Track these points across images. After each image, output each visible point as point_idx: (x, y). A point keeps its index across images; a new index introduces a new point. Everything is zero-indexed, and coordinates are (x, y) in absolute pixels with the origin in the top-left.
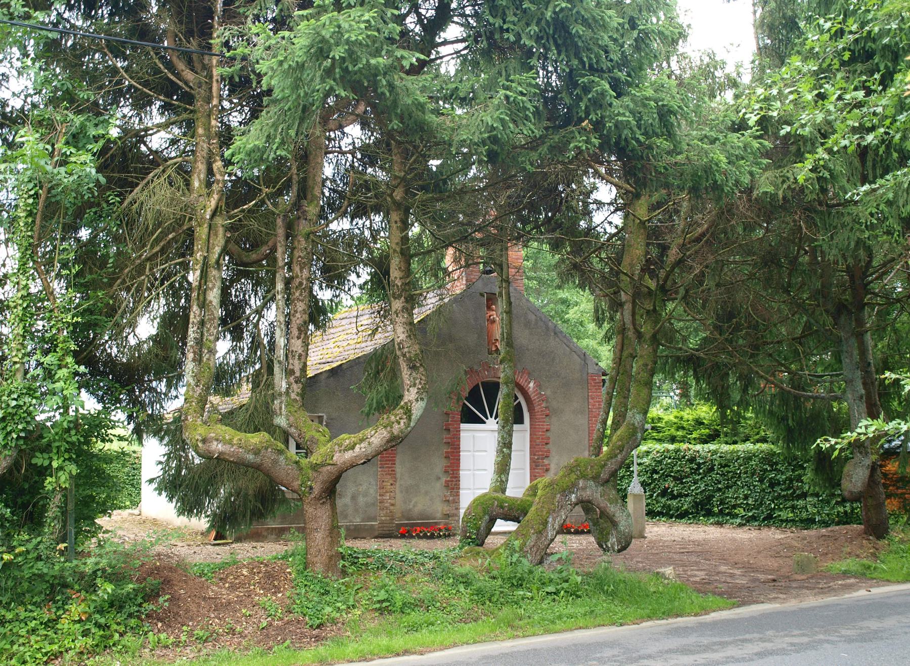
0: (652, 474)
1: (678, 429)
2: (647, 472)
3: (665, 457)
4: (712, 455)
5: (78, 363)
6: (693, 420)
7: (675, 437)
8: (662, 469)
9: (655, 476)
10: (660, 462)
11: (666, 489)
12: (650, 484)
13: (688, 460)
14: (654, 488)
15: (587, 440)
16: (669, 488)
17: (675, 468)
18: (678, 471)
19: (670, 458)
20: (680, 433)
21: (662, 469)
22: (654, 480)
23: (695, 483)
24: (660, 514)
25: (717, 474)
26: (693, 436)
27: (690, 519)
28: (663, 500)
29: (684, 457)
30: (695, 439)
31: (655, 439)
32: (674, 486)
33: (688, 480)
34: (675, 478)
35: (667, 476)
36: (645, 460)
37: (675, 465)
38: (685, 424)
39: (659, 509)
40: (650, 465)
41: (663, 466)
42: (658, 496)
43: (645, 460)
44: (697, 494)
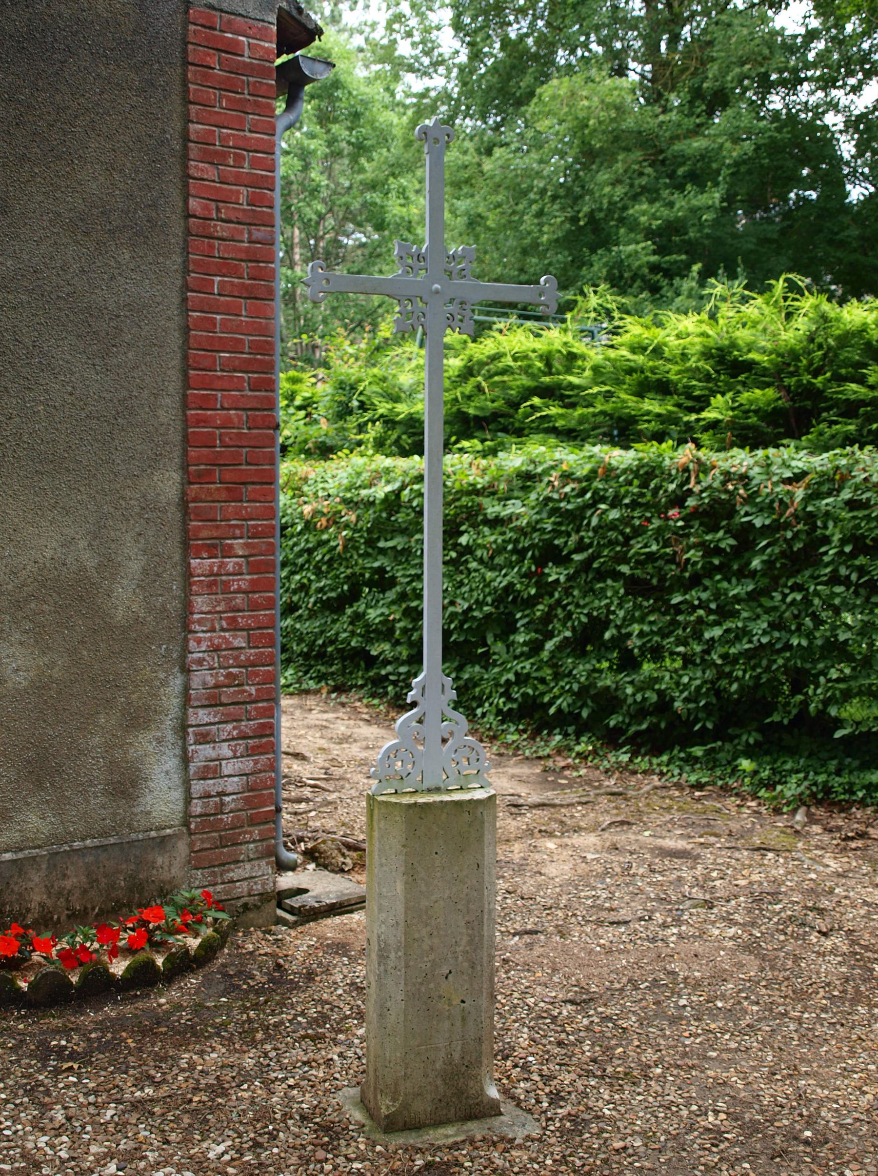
0: (541, 562)
1: (641, 391)
2: (521, 553)
3: (598, 498)
4: (814, 496)
5: (862, 534)
6: (706, 354)
7: (632, 420)
8: (580, 547)
9: (554, 573)
10: (576, 518)
11: (598, 624)
12: (531, 603)
13: (695, 513)
14: (548, 618)
15: (170, 403)
16: (605, 624)
17: (637, 546)
18: (651, 557)
19: (615, 503)
20: (652, 405)
21: (580, 547)
22: (546, 588)
23: (725, 612)
24: (562, 720)
25: (834, 579)
26: (709, 415)
27: (692, 761)
28: (582, 670)
29: (678, 500)
30: (714, 425)
31: (554, 431)
32: (630, 619)
33: (694, 595)
34: (635, 587)
35: (601, 575)
36: (515, 507)
37: (638, 532)
38: (673, 371)
39: (563, 702)
40: (534, 527)
41: (588, 536)
42: (559, 648)
43: (515, 507)
44: (731, 661)
